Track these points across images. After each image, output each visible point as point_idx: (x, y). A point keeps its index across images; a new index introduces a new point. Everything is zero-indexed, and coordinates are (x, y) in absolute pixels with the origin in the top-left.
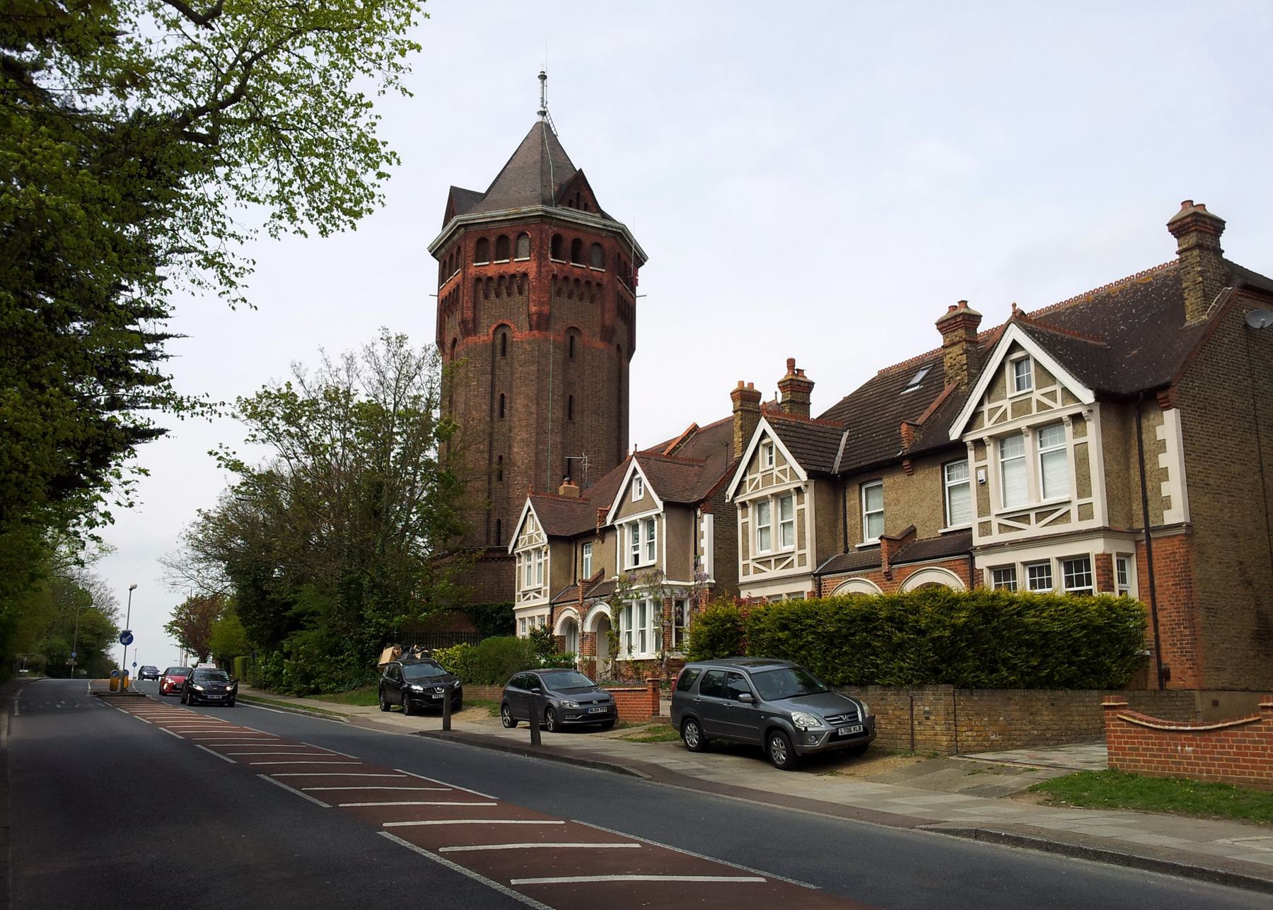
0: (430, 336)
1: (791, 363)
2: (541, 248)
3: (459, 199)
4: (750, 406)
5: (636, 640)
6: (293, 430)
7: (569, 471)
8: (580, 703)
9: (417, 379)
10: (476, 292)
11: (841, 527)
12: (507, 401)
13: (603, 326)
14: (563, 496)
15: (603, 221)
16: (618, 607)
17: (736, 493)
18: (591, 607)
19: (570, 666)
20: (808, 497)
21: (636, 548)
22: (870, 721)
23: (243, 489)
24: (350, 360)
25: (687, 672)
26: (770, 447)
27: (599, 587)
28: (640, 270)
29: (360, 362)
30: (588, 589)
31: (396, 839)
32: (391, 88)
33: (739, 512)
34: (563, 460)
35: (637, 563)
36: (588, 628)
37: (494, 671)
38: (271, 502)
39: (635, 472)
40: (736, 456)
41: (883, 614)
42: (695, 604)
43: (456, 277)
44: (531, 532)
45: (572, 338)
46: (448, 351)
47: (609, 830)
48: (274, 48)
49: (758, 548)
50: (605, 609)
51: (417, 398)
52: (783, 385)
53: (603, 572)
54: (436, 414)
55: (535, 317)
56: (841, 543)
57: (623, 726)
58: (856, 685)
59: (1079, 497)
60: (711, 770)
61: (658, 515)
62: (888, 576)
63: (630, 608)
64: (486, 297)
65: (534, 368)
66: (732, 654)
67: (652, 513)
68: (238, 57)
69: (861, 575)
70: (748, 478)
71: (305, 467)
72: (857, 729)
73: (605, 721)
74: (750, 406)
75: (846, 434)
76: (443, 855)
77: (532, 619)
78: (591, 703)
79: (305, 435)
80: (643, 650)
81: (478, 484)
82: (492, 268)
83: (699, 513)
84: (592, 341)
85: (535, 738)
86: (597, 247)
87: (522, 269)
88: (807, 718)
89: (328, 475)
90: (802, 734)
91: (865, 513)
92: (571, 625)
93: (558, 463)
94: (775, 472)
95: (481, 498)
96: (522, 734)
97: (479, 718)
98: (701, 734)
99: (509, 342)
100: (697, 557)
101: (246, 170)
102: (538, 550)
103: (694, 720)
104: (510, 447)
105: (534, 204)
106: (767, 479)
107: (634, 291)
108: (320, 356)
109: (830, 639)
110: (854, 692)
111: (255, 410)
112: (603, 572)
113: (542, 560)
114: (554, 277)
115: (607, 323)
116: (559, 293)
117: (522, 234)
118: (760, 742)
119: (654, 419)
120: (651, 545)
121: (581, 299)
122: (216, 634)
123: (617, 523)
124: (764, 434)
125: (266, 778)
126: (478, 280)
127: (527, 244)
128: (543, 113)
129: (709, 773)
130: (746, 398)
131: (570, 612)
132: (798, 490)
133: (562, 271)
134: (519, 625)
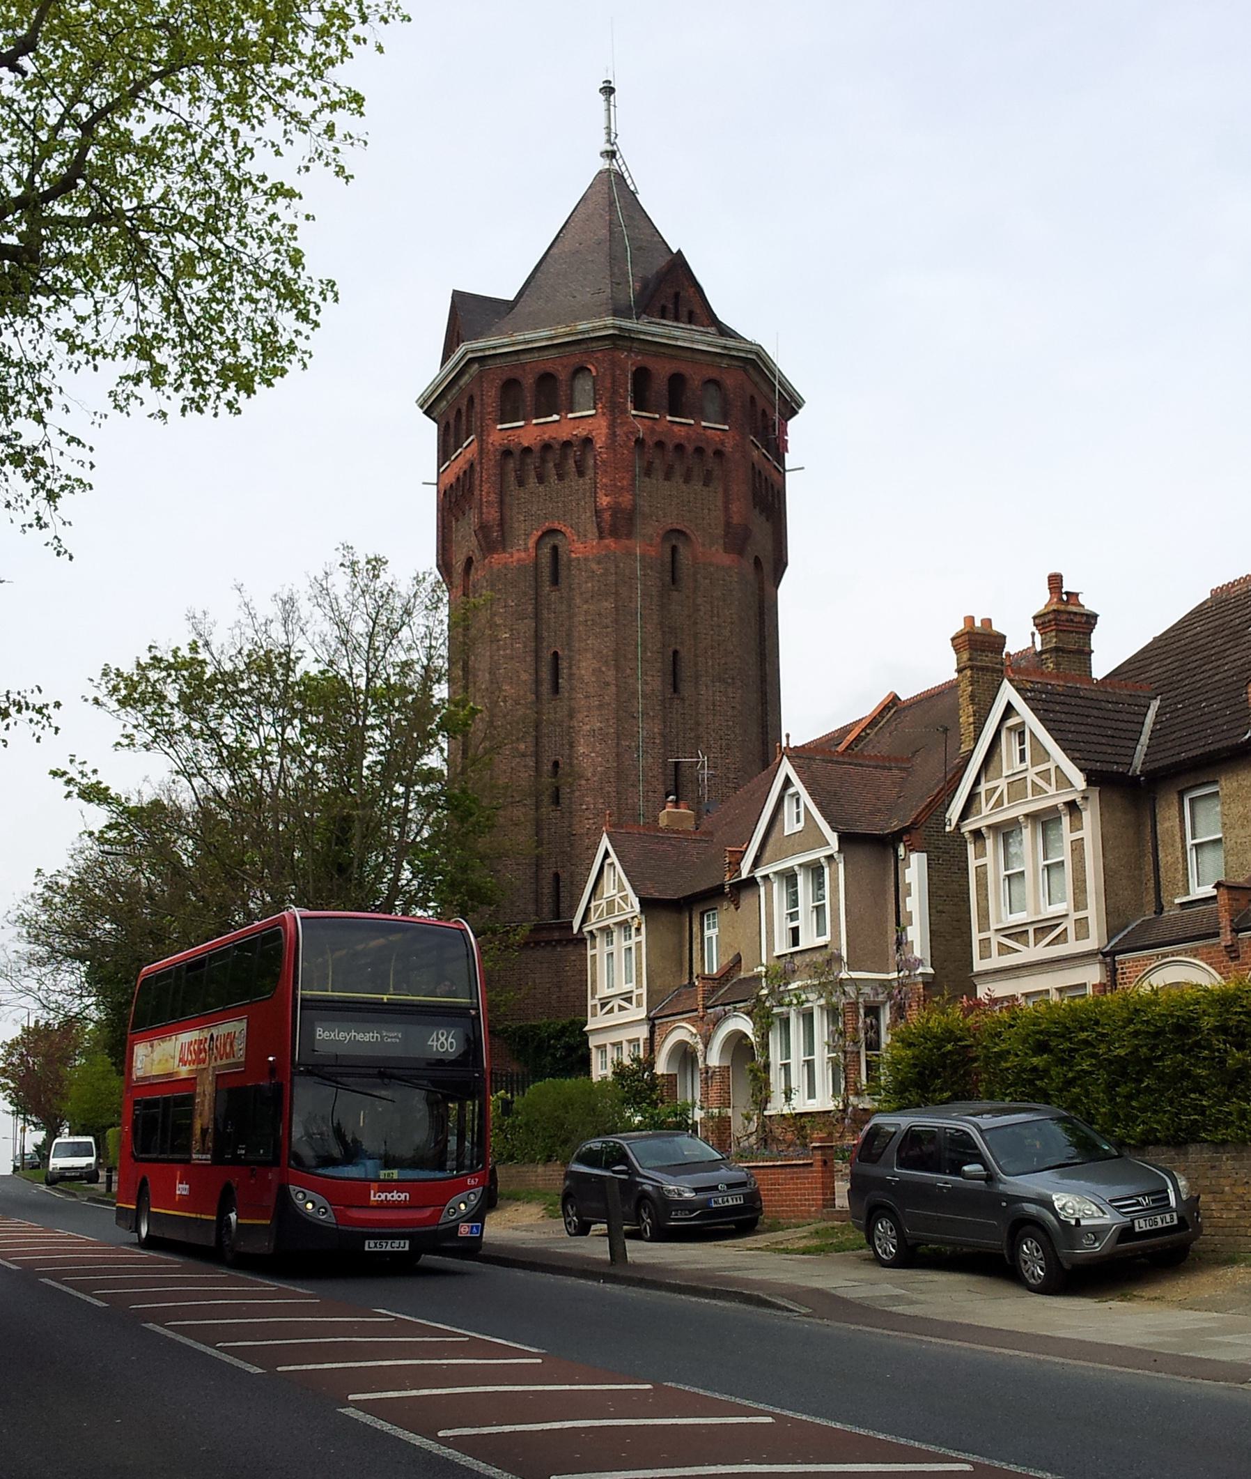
0: (425, 556)
1: (1055, 581)
2: (615, 392)
3: (468, 314)
4: (986, 659)
5: (798, 1078)
6: (196, 725)
7: (677, 784)
8: (696, 1190)
9: (405, 633)
10: (502, 475)
11: (1149, 868)
12: (564, 664)
13: (728, 524)
14: (668, 829)
15: (722, 341)
16: (764, 1021)
17: (964, 815)
18: (718, 1021)
19: (684, 1126)
20: (1090, 817)
21: (793, 916)
22: (1191, 1205)
23: (112, 834)
24: (289, 604)
25: (876, 1132)
26: (1020, 730)
27: (732, 987)
28: (792, 424)
29: (305, 608)
30: (713, 991)
31: (368, 1419)
32: (317, 166)
33: (971, 848)
34: (665, 763)
35: (795, 942)
36: (714, 1060)
37: (554, 1140)
38: (163, 855)
39: (788, 782)
40: (964, 748)
41: (1207, 1023)
42: (900, 1011)
43: (468, 450)
44: (612, 894)
45: (674, 549)
46: (458, 580)
47: (725, 1397)
48: (126, 100)
49: (1005, 910)
50: (745, 1025)
51: (406, 666)
52: (1042, 622)
53: (737, 960)
54: (441, 691)
55: (607, 516)
56: (1151, 896)
57: (772, 1228)
58: (1167, 1144)
59: (1077, 909)
60: (915, 1296)
61: (830, 858)
62: (1232, 952)
63: (786, 1023)
64: (521, 483)
65: (608, 605)
66: (956, 1097)
67: (819, 854)
68: (67, 114)
69: (1185, 952)
70: (983, 788)
71: (217, 792)
72: (1170, 1219)
73: (740, 1220)
74: (986, 659)
75: (1155, 705)
76: (445, 1441)
77: (618, 1045)
78: (715, 1188)
79: (215, 735)
80: (812, 1094)
81: (518, 813)
82: (529, 431)
83: (901, 851)
84: (709, 553)
85: (617, 1253)
86: (712, 390)
87: (581, 431)
88: (1080, 1203)
89: (258, 802)
90: (1072, 1231)
91: (1190, 842)
92: (685, 1055)
93: (657, 770)
94: (1031, 775)
95: (523, 838)
96: (596, 1247)
97: (526, 1221)
98: (900, 1236)
99: (563, 559)
100: (900, 926)
101: (82, 305)
102: (625, 925)
103: (890, 1213)
104: (571, 745)
105: (598, 315)
106: (1017, 788)
107: (781, 461)
108: (235, 598)
109: (1121, 1069)
110: (1163, 1155)
111: (133, 692)
112: (737, 960)
113: (631, 943)
114: (640, 442)
115: (736, 520)
116: (648, 472)
117: (581, 370)
118: (1003, 1245)
119: (818, 695)
120: (819, 910)
121: (687, 480)
122: (73, 1092)
123: (759, 874)
124: (1009, 710)
125: (158, 1329)
126: (507, 453)
127: (588, 386)
128: (611, 155)
129: (912, 1302)
130: (979, 644)
131: (683, 1032)
132: (1072, 806)
133: (652, 431)
134: (596, 1058)
